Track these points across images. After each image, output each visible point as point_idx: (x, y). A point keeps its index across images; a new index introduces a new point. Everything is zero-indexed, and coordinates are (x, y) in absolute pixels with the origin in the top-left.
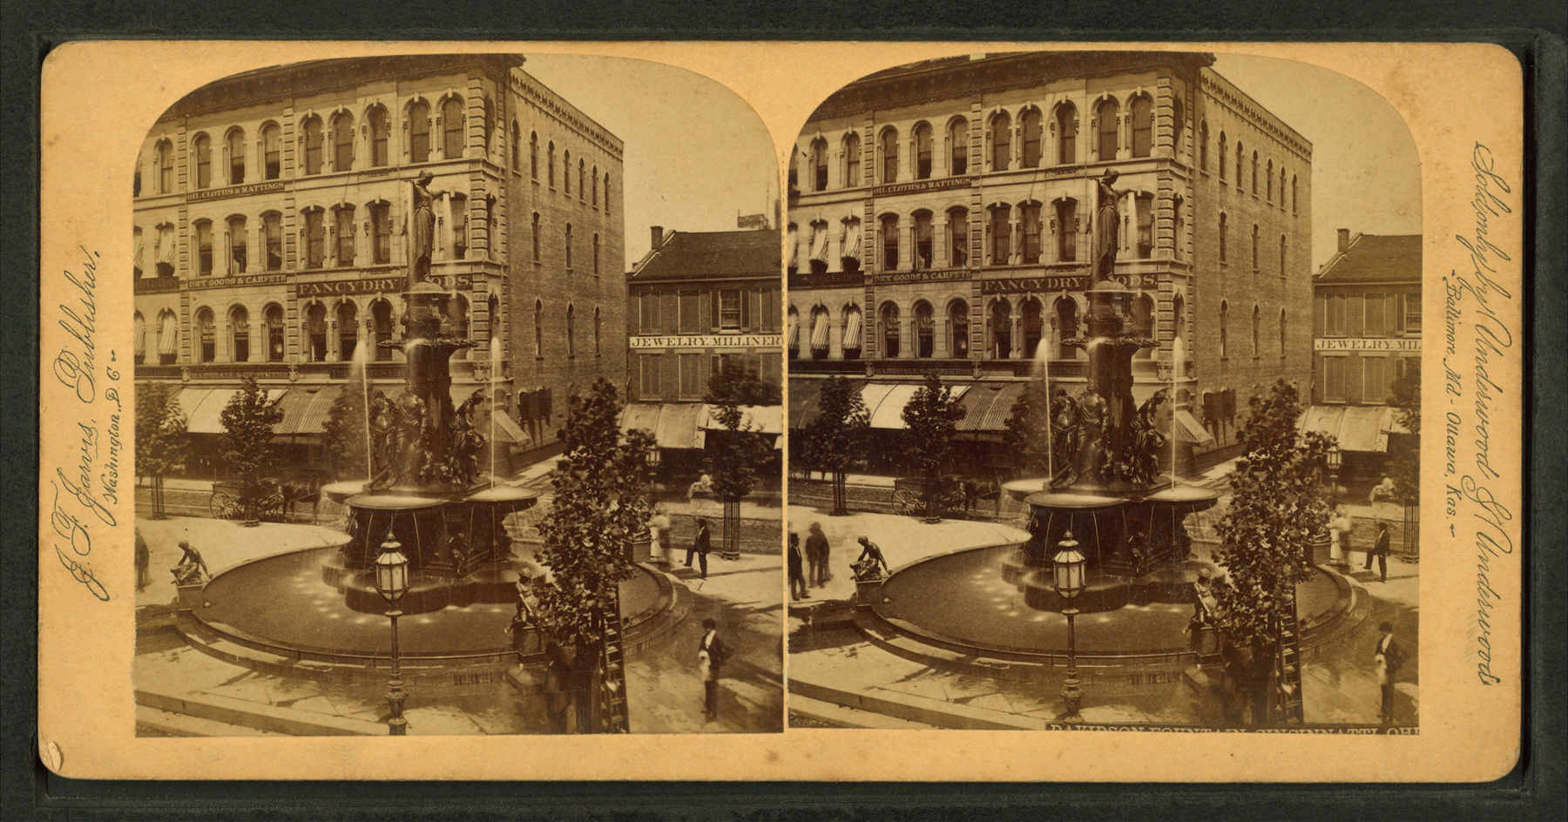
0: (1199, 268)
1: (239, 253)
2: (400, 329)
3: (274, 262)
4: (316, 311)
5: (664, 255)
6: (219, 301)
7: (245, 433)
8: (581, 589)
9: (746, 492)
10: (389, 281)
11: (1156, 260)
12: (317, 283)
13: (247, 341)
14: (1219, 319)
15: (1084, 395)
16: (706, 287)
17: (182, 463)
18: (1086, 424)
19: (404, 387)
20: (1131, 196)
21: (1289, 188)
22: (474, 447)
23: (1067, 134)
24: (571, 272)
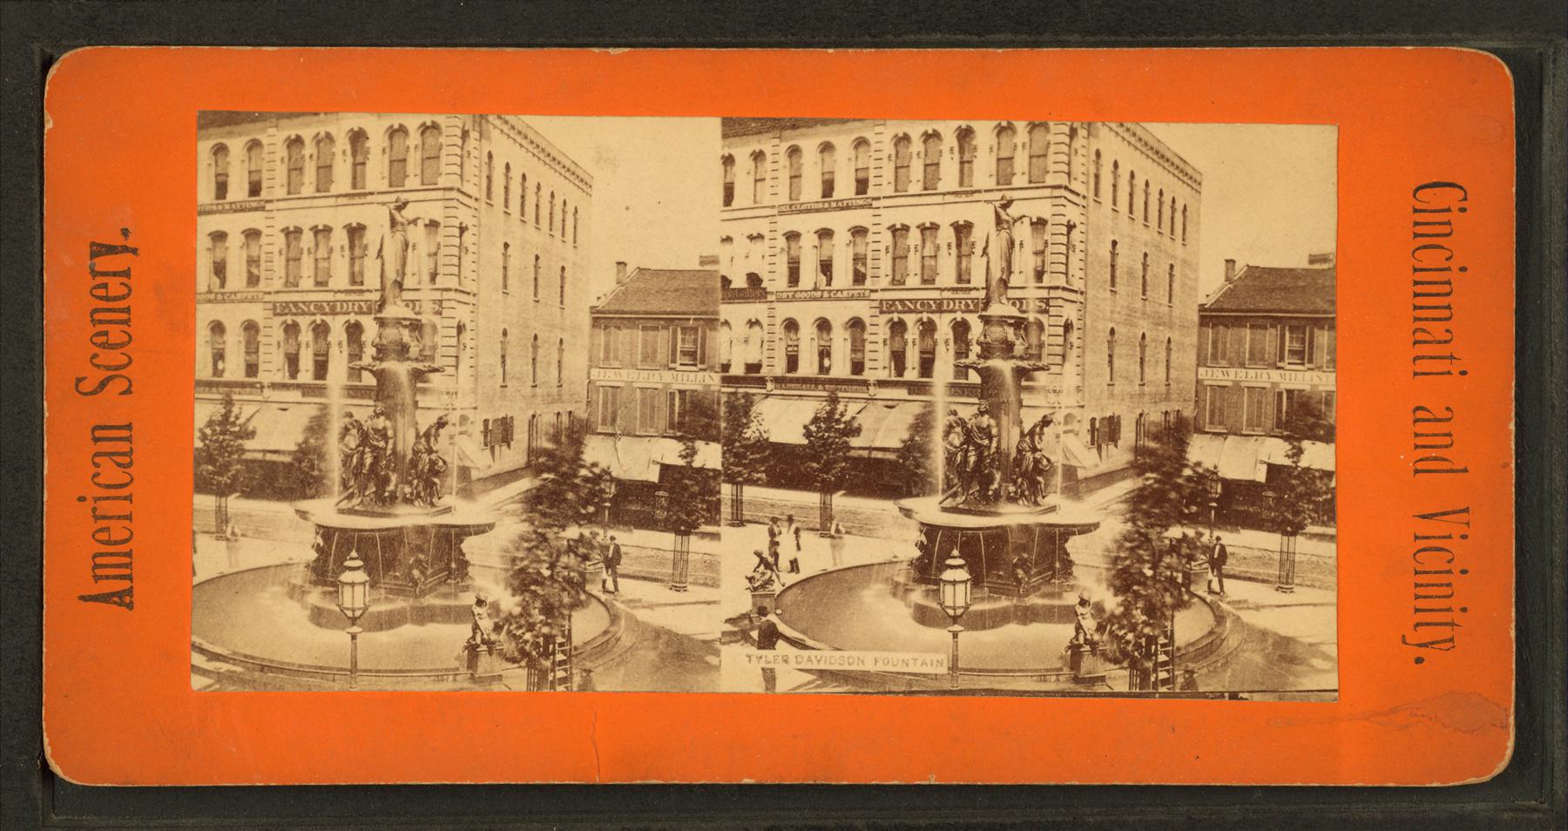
0: (1091, 293)
1: (826, 267)
3: (859, 278)
4: (898, 328)
6: (806, 314)
7: (824, 445)
8: (1139, 616)
10: (969, 302)
11: (1048, 285)
12: (900, 300)
13: (797, 356)
15: (976, 416)
16: (1275, 322)
17: (763, 472)
18: (975, 444)
21: (1179, 216)
22: (1042, 470)
23: (966, 158)
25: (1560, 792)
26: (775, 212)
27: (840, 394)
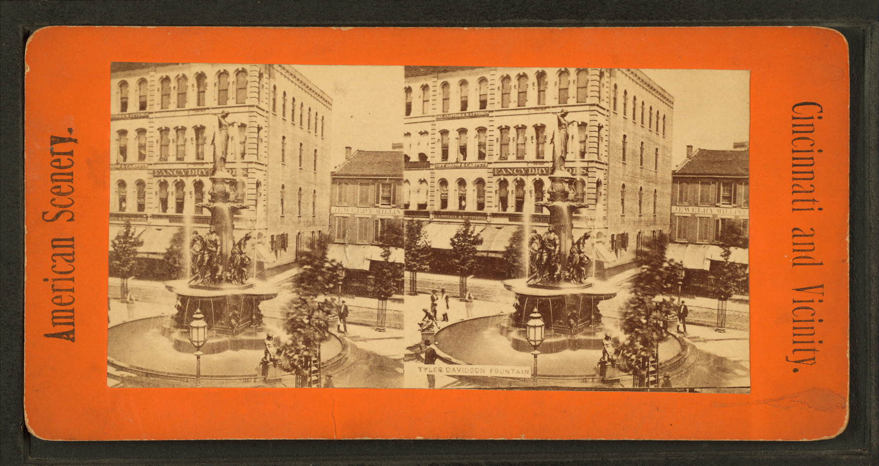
1: (463, 150)
2: (547, 196)
3: (482, 156)
4: (503, 184)
5: (693, 161)
6: (452, 176)
7: (462, 250)
8: (639, 346)
9: (731, 296)
10: (543, 169)
12: (504, 168)
14: (620, 193)
15: (547, 233)
16: (715, 180)
17: (428, 264)
18: (547, 249)
19: (547, 228)
20: (575, 124)
21: (661, 121)
23: (541, 89)
24: (642, 168)
25: (875, 444)
26: (434, 119)
27: (471, 221)
